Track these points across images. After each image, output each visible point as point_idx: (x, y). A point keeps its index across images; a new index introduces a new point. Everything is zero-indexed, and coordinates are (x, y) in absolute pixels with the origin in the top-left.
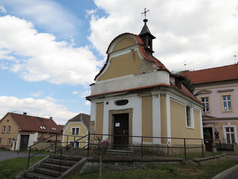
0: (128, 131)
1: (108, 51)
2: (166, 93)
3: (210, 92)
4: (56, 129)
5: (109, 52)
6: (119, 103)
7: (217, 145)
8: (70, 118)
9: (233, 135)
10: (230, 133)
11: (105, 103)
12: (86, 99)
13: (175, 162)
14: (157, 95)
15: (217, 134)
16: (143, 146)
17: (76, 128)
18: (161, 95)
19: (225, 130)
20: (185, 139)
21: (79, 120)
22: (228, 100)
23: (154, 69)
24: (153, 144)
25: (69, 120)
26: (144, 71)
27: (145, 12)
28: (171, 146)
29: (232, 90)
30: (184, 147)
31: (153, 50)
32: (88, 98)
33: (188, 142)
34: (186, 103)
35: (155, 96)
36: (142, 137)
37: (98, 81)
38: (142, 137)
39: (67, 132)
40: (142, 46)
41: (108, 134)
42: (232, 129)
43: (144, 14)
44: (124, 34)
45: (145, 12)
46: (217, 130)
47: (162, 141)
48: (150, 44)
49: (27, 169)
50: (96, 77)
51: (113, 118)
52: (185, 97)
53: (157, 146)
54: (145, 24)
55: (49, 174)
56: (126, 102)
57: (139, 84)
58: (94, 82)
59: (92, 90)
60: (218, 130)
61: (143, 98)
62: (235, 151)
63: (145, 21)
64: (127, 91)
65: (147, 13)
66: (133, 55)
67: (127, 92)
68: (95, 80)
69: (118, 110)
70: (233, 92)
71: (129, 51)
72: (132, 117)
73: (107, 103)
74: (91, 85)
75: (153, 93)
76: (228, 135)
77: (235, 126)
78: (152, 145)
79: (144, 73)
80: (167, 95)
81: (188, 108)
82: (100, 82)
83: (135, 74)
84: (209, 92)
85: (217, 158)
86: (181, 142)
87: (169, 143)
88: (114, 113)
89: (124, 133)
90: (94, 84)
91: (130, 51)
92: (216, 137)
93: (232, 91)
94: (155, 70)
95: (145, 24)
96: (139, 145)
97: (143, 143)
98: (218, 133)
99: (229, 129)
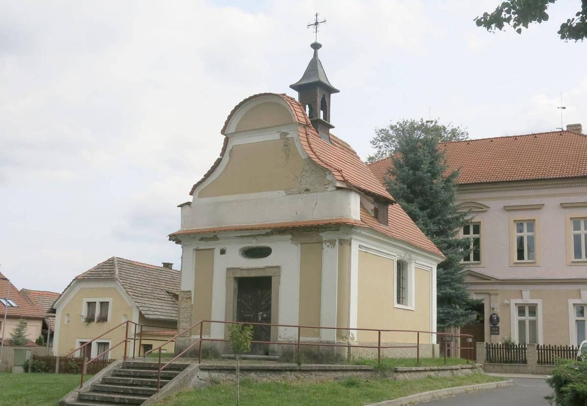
0: (270, 315)
1: (225, 127)
2: (350, 237)
3: (485, 209)
4: (14, 305)
5: (227, 132)
6: (251, 253)
7: (541, 349)
8: (79, 272)
9: (533, 324)
10: (527, 318)
11: (217, 252)
12: (168, 238)
13: (358, 373)
14: (332, 242)
15: (494, 321)
16: (300, 343)
17: (98, 300)
18: (342, 242)
19: (514, 311)
20: (379, 331)
21: (111, 279)
22: (528, 231)
23: (329, 184)
24: (321, 342)
25: (76, 279)
26: (308, 186)
27: (317, 24)
28: (356, 344)
29: (538, 207)
30: (378, 346)
31: (332, 123)
32: (175, 238)
33: (386, 339)
34: (396, 254)
35: (328, 244)
36: (299, 327)
37: (200, 196)
38: (299, 327)
39: (68, 315)
40: (305, 127)
41: (223, 320)
42: (533, 310)
43: (312, 28)
44: (265, 94)
45: (317, 24)
46: (495, 310)
47: (339, 336)
48: (325, 107)
49: (81, 387)
50: (195, 187)
51: (236, 286)
52: (398, 244)
53: (330, 345)
54: (315, 55)
55: (131, 392)
56: (264, 252)
57: (297, 213)
58: (190, 199)
59: (183, 216)
60: (498, 311)
61: (303, 245)
62: (528, 362)
63: (316, 46)
64: (270, 228)
65: (320, 26)
66: (286, 145)
67: (269, 231)
68: (191, 194)
69: (248, 270)
70: (540, 211)
71: (273, 136)
72: (280, 284)
73: (223, 252)
74: (181, 206)
75: (325, 236)
76: (521, 324)
77: (539, 302)
78: (318, 342)
79: (307, 190)
80: (353, 242)
81: (401, 266)
82: (205, 200)
83: (289, 192)
84: (483, 209)
85: (452, 370)
86: (372, 338)
87: (353, 339)
88: (239, 275)
89: (260, 319)
90: (189, 204)
91: (277, 136)
92: (491, 330)
93: (540, 209)
94: (331, 188)
95: (315, 55)
96: (294, 342)
97: (302, 339)
98: (498, 319)
99: (524, 307)
